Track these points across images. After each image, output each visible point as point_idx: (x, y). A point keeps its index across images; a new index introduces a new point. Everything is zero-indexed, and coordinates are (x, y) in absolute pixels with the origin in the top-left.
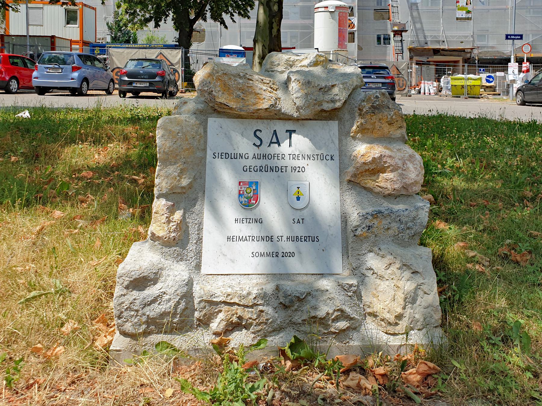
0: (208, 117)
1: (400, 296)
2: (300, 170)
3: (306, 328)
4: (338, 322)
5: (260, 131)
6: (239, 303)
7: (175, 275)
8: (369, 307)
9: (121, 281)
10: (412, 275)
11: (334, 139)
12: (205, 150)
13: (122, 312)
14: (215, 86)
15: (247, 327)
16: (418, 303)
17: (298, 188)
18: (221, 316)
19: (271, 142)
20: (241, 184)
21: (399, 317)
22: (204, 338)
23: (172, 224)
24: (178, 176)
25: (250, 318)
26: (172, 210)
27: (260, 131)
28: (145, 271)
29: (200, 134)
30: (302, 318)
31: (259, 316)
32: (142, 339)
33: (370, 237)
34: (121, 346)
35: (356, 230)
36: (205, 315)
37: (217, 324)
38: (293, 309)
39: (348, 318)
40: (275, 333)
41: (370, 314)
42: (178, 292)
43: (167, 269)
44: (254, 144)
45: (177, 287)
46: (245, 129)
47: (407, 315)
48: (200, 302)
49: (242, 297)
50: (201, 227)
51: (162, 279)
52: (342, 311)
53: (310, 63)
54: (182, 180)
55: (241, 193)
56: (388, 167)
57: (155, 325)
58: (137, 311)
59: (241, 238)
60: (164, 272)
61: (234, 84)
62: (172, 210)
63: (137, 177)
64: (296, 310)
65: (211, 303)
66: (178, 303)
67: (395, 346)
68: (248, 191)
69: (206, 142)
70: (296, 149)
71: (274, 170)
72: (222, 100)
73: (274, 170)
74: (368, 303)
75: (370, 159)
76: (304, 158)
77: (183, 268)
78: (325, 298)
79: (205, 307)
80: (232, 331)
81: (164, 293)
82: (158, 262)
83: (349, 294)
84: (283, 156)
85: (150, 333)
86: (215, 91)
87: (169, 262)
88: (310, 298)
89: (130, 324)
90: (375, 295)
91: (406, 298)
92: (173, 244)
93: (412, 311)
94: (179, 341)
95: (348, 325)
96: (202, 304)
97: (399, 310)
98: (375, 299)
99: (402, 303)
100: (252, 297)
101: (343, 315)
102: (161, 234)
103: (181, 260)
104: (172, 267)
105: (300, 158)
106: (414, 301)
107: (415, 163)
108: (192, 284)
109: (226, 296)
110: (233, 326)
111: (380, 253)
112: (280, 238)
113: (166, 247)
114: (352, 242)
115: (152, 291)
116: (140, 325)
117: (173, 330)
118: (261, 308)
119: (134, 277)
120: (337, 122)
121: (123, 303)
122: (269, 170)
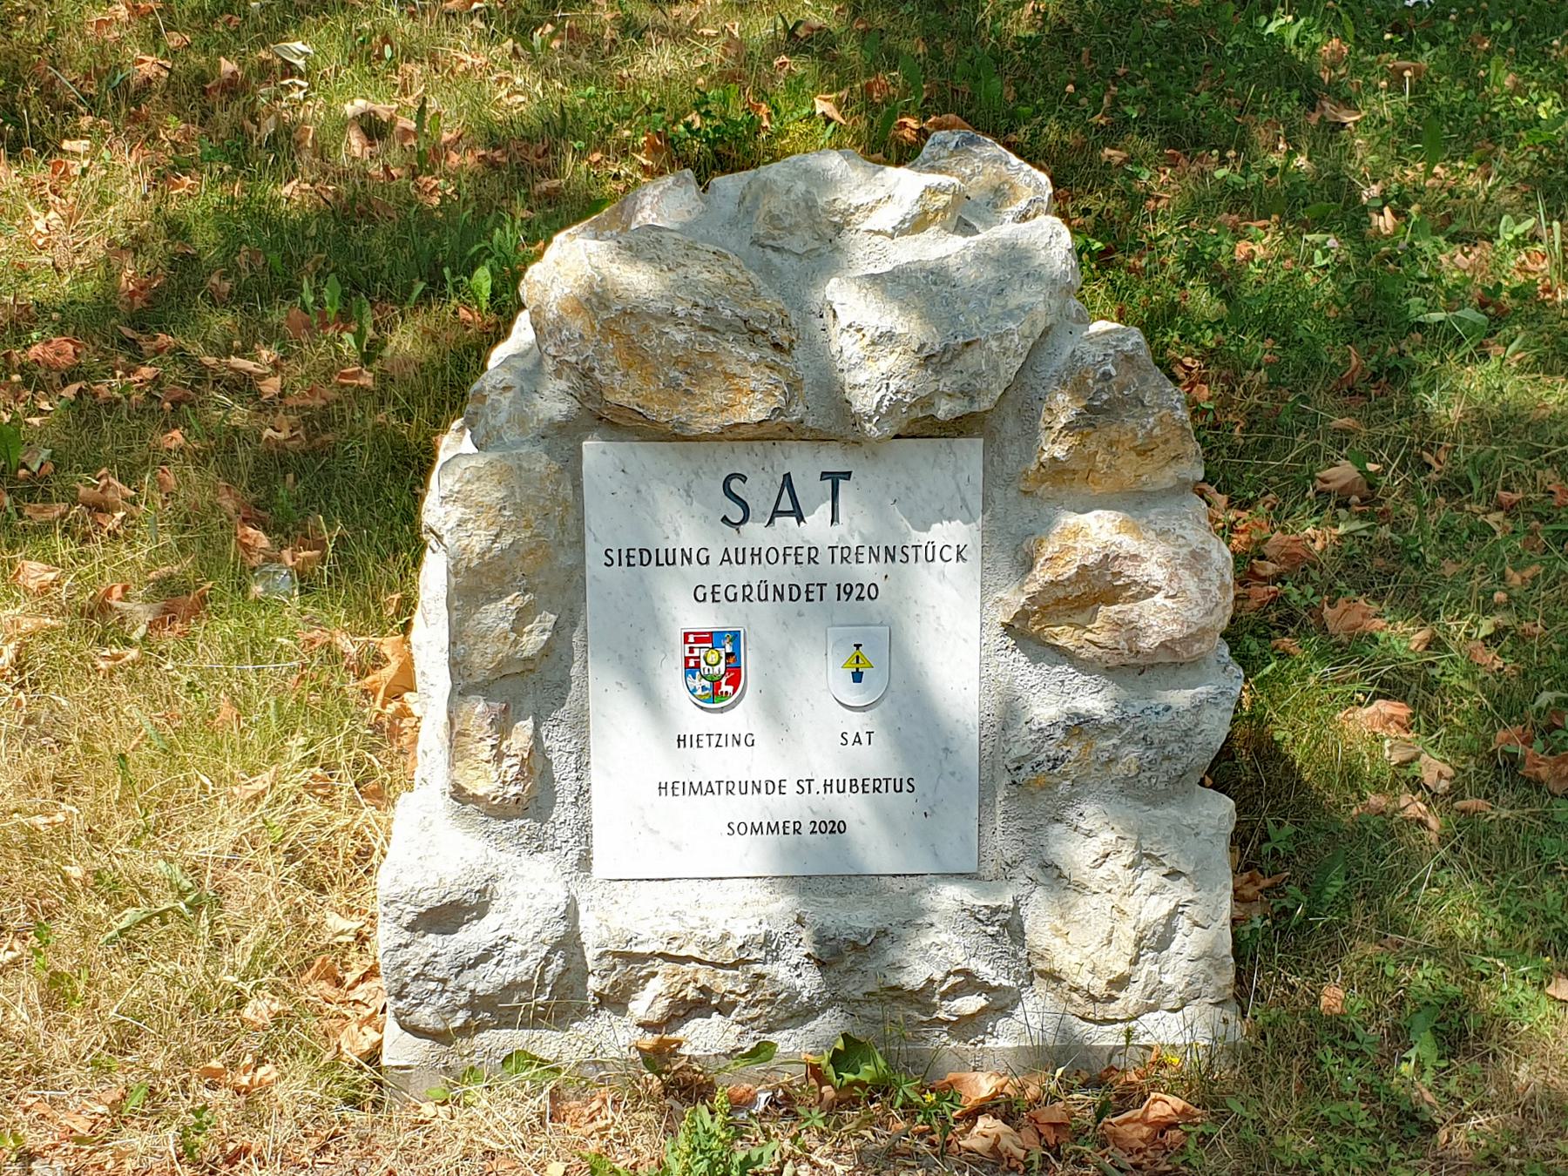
0: (581, 440)
1: (1126, 935)
2: (865, 594)
3: (875, 1011)
4: (956, 997)
5: (744, 479)
6: (702, 957)
7: (528, 895)
8: (1042, 958)
9: (393, 911)
10: (1165, 880)
11: (969, 497)
12: (580, 543)
13: (405, 985)
14: (601, 354)
15: (724, 1009)
16: (1174, 947)
17: (858, 646)
18: (656, 986)
19: (776, 513)
20: (691, 638)
21: (1121, 982)
22: (618, 1036)
23: (507, 762)
24: (513, 630)
25: (731, 992)
26: (502, 726)
27: (744, 479)
28: (455, 888)
29: (565, 500)
30: (865, 989)
31: (752, 987)
32: (461, 1042)
33: (1057, 785)
34: (412, 1057)
35: (1019, 768)
36: (615, 984)
37: (648, 1002)
38: (843, 967)
39: (983, 988)
40: (793, 1022)
41: (1042, 974)
42: (543, 936)
43: (507, 876)
44: (725, 519)
45: (539, 923)
46: (697, 474)
47: (1141, 977)
48: (602, 956)
49: (706, 944)
50: (584, 759)
51: (497, 905)
52: (966, 973)
53: (902, 222)
54: (525, 639)
55: (692, 663)
56: (1126, 587)
57: (495, 1009)
58: (444, 981)
59: (696, 786)
60: (500, 887)
61: (660, 345)
62: (502, 726)
63: (247, 365)
64: (850, 970)
65: (629, 958)
66: (547, 960)
67: (1102, 1048)
68: (713, 657)
69: (581, 519)
70: (851, 532)
71: (786, 595)
72: (623, 398)
73: (786, 595)
74: (1039, 950)
75: (1071, 570)
76: (877, 559)
77: (550, 873)
78: (925, 942)
79: (614, 967)
80: (686, 1018)
81: (509, 939)
82: (482, 861)
83: (990, 930)
84: (813, 553)
85: (480, 1028)
86: (601, 370)
87: (509, 856)
88: (885, 942)
89: (429, 1010)
90: (1058, 930)
91: (1141, 939)
92: (515, 812)
93: (1156, 968)
94: (548, 1043)
95: (984, 1003)
96: (606, 962)
97: (1121, 967)
98: (1058, 941)
99: (1130, 949)
100: (733, 944)
101: (969, 982)
102: (481, 788)
103: (540, 849)
104: (519, 871)
105: (865, 557)
106: (1163, 943)
107: (1205, 575)
108: (577, 913)
109: (665, 940)
110: (684, 1009)
111: (1082, 824)
112: (805, 785)
113: (498, 818)
114: (1006, 798)
115: (475, 936)
116: (454, 1012)
117: (535, 1020)
118: (757, 968)
119: (427, 905)
120: (981, 440)
121: (404, 964)
122: (770, 597)
